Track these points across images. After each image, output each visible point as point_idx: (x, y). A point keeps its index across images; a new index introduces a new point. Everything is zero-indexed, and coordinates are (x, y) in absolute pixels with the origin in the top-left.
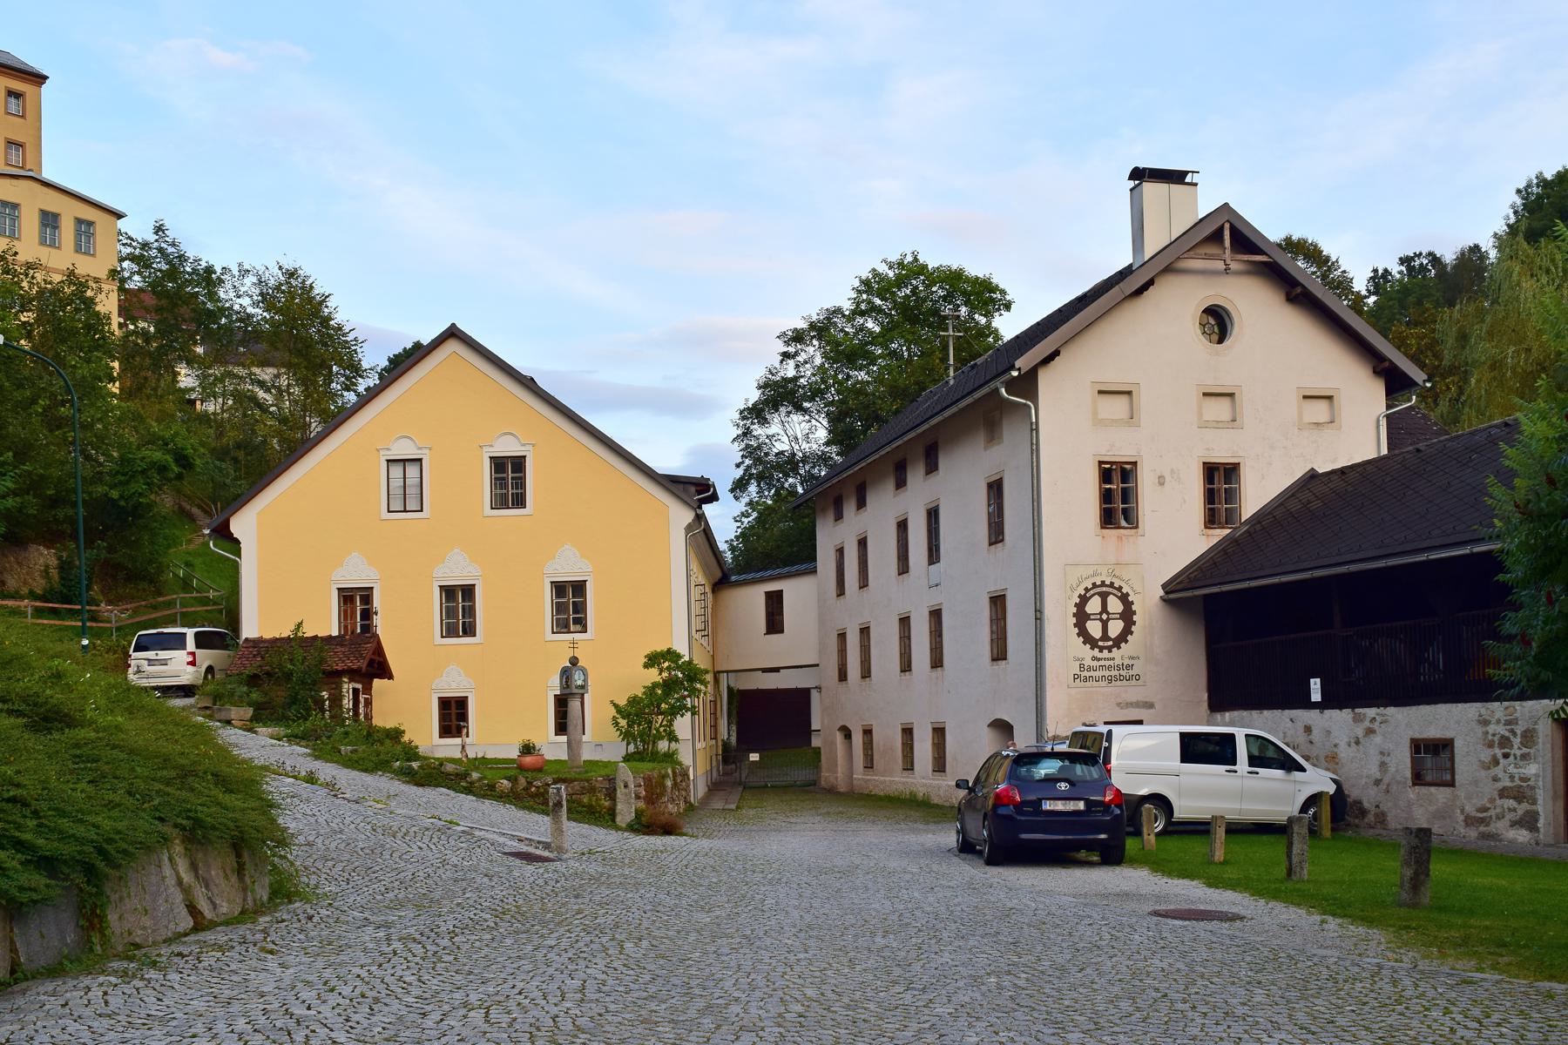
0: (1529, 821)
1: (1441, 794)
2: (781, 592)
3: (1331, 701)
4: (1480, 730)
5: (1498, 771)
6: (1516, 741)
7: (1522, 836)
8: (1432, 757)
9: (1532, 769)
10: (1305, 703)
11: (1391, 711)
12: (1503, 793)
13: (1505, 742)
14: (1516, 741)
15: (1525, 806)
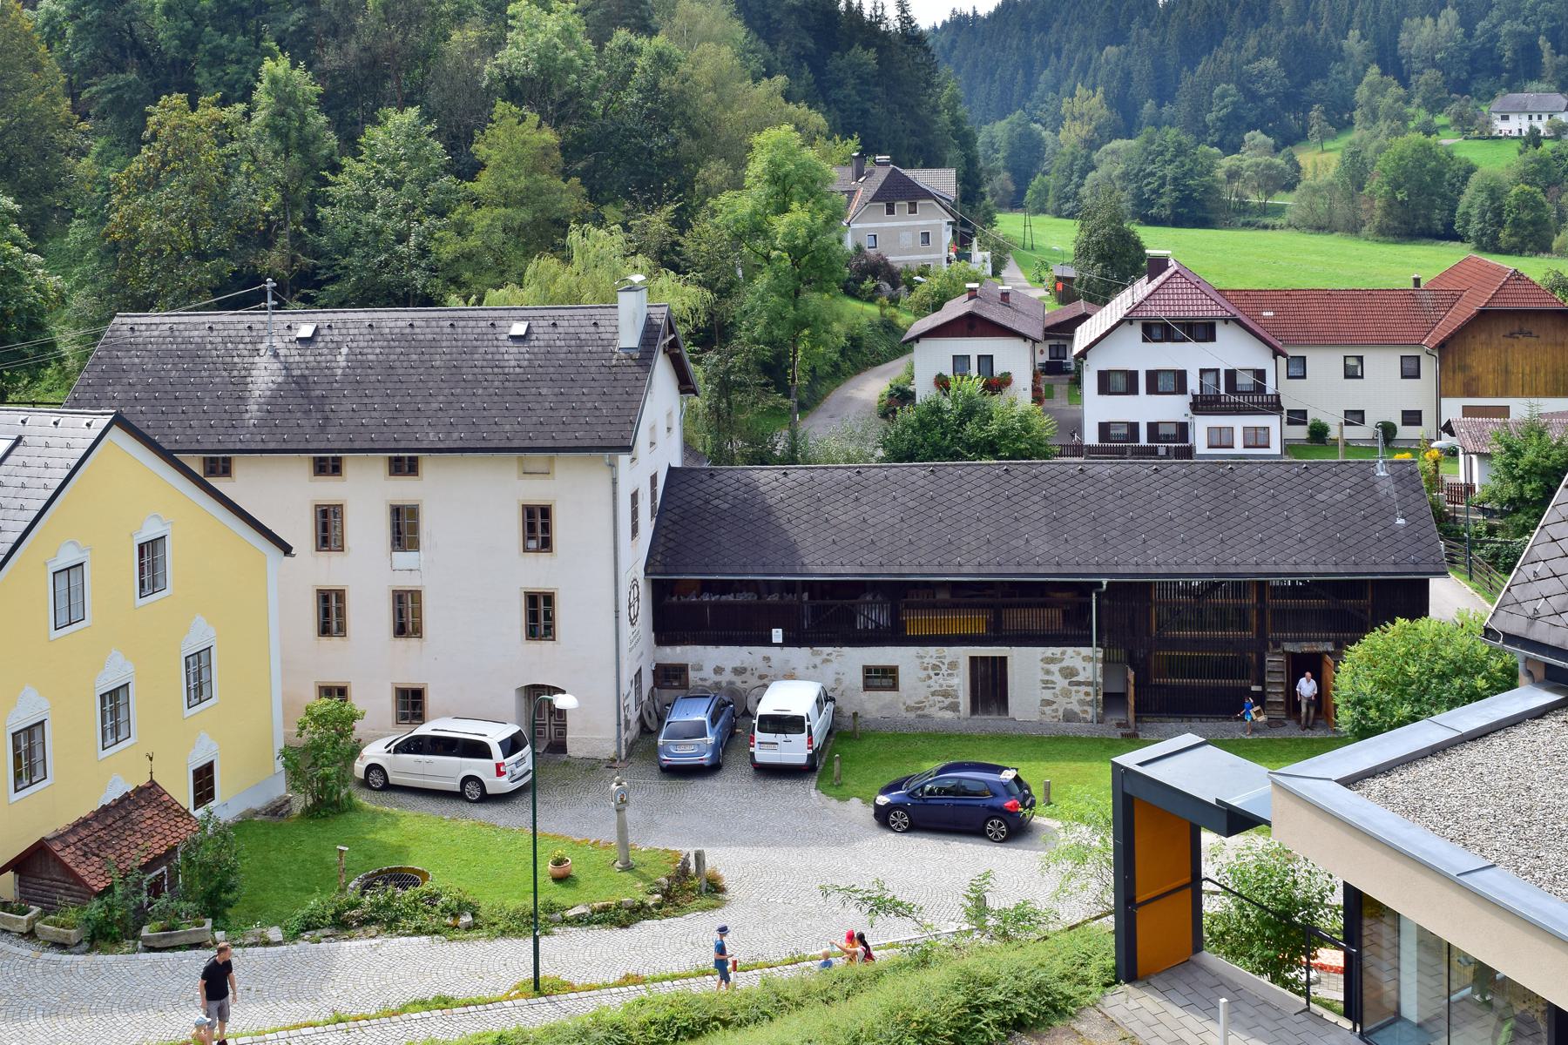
0: (954, 707)
1: (887, 696)
2: (1004, 659)
3: (788, 642)
4: (918, 661)
5: (931, 682)
6: (944, 668)
7: (949, 715)
8: (1063, 653)
9: (955, 681)
10: (767, 641)
11: (846, 650)
12: (933, 694)
13: (935, 667)
14: (944, 668)
15: (950, 700)
